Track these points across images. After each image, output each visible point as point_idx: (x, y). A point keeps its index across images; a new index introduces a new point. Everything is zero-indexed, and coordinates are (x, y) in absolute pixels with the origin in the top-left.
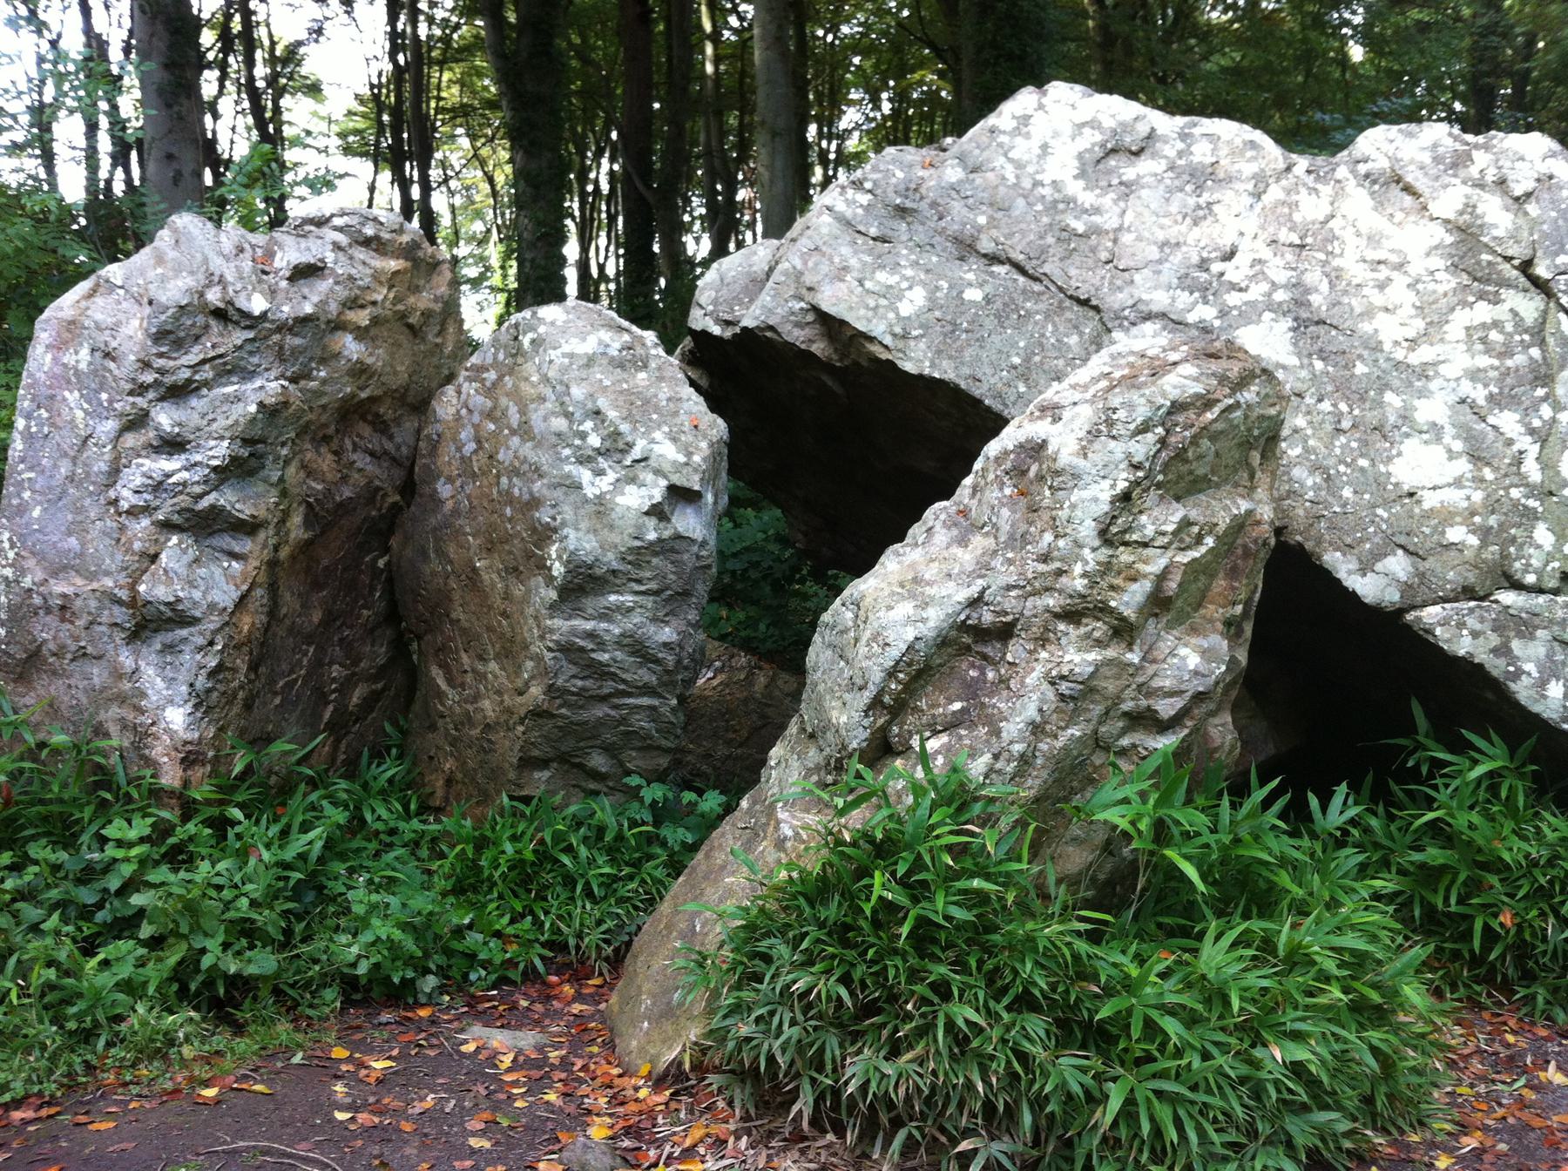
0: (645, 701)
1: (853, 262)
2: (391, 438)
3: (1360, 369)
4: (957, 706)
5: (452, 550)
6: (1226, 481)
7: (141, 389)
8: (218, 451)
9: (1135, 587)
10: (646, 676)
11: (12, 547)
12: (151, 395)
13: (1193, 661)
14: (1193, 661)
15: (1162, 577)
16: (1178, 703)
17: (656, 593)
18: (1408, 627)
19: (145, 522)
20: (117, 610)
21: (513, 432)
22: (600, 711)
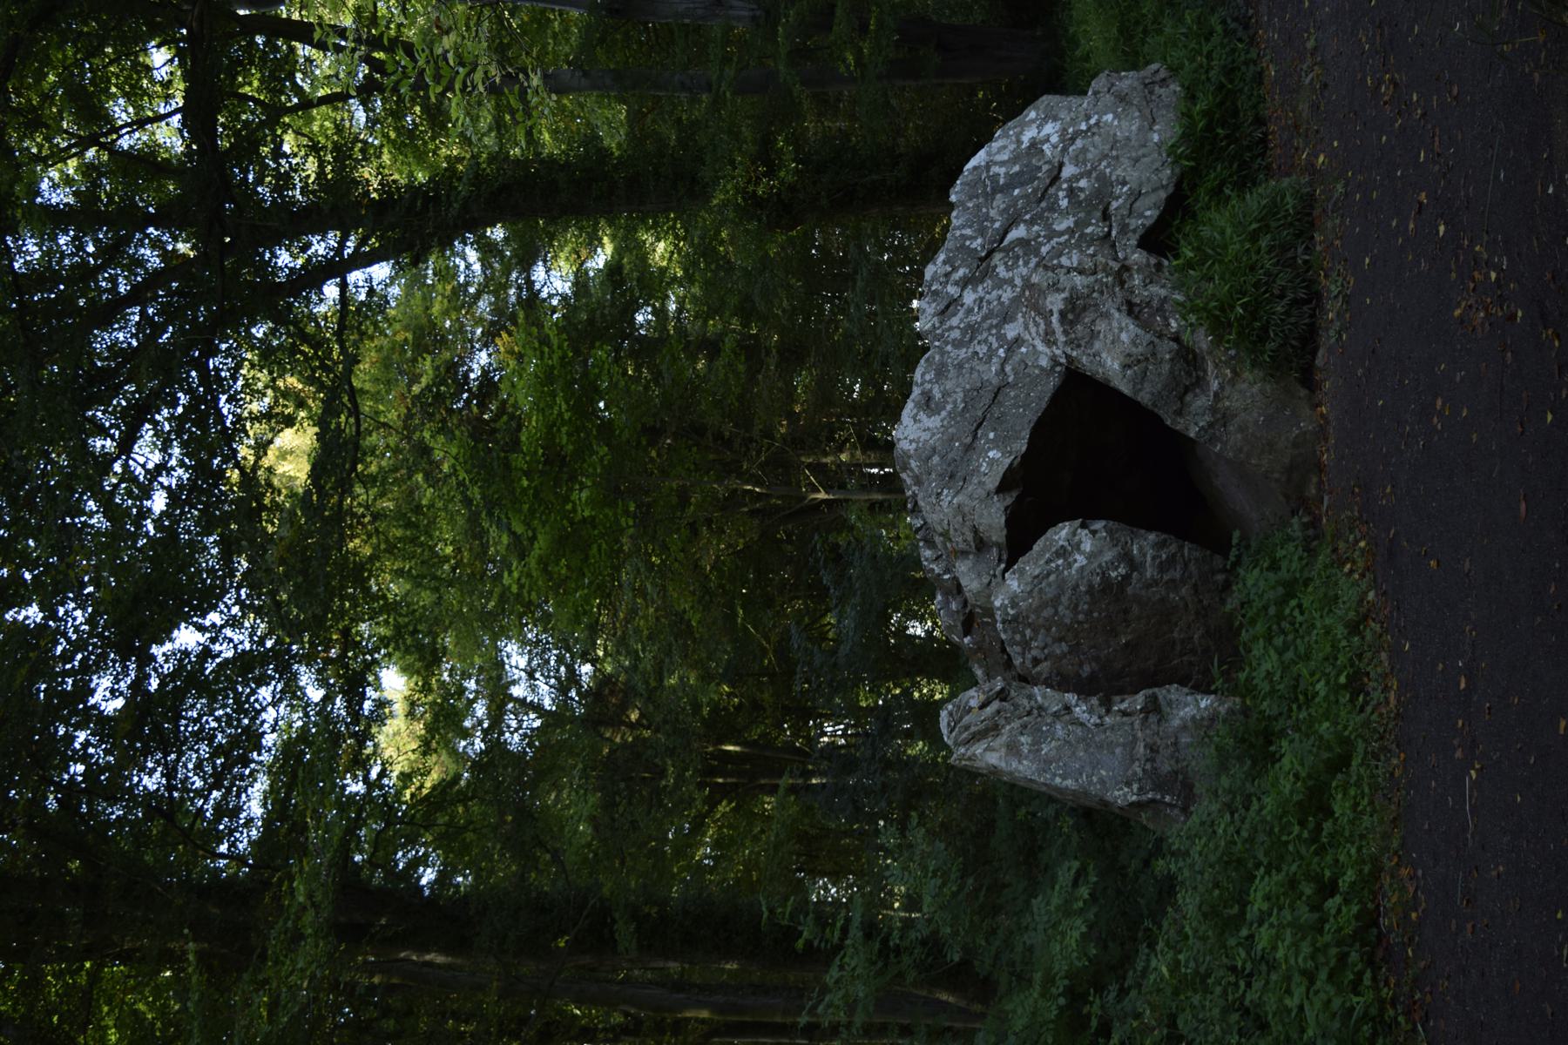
22: (1192, 567)
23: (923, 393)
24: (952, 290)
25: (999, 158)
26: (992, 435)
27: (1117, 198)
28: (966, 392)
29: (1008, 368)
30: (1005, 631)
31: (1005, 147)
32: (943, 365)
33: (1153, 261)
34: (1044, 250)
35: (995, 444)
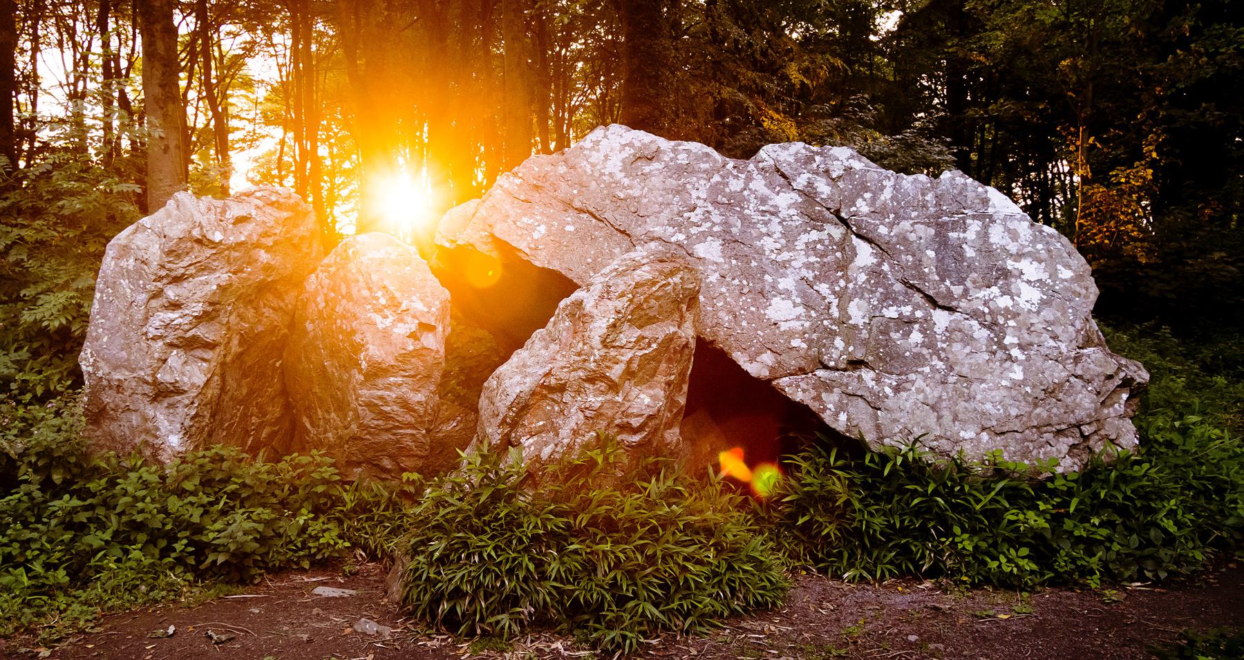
0: (410, 431)
1: (511, 212)
2: (283, 300)
3: (754, 264)
4: (541, 423)
5: (313, 357)
6: (667, 318)
7: (160, 278)
8: (198, 308)
9: (617, 366)
10: (409, 418)
12: (165, 281)
13: (647, 400)
14: (647, 400)
15: (630, 362)
16: (641, 420)
17: (414, 376)
18: (773, 388)
19: (160, 343)
20: (146, 386)
21: (343, 297)
22: (386, 436)
23: (658, 150)
27: (878, 380)
28: (637, 200)
32: (693, 172)
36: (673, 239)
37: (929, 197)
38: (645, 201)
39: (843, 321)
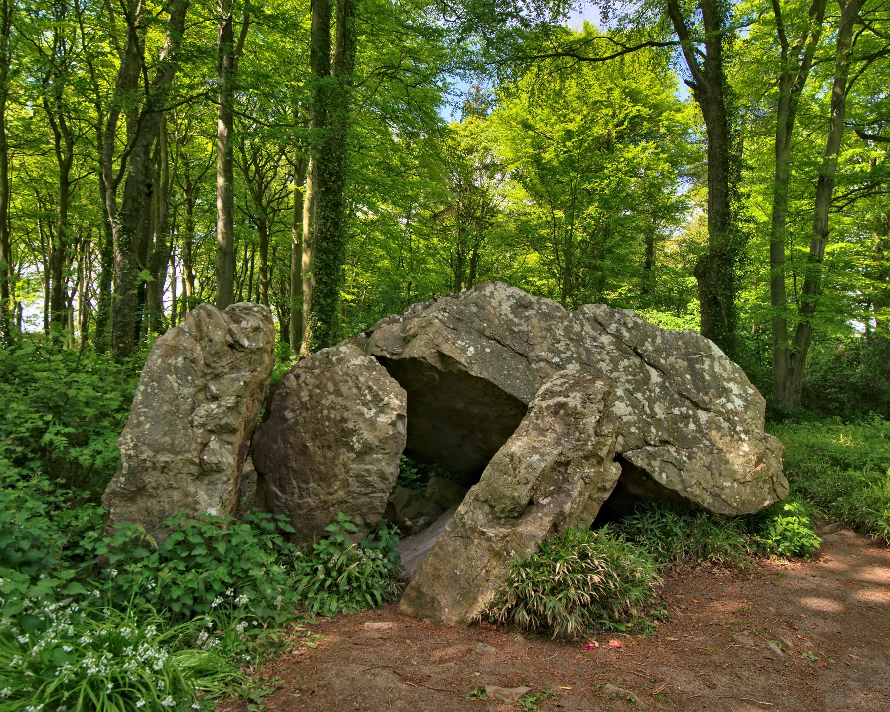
0: (380, 495)
8: (231, 401)
11: (132, 441)
12: (208, 377)
20: (192, 467)
22: (363, 500)
23: (530, 302)
24: (613, 327)
25: (717, 365)
26: (488, 350)
27: (677, 452)
29: (542, 364)
30: (322, 354)
31: (725, 370)
32: (553, 318)
33: (608, 485)
34: (639, 395)
35: (480, 352)
36: (554, 361)
37: (680, 343)
38: (531, 334)
39: (653, 415)
